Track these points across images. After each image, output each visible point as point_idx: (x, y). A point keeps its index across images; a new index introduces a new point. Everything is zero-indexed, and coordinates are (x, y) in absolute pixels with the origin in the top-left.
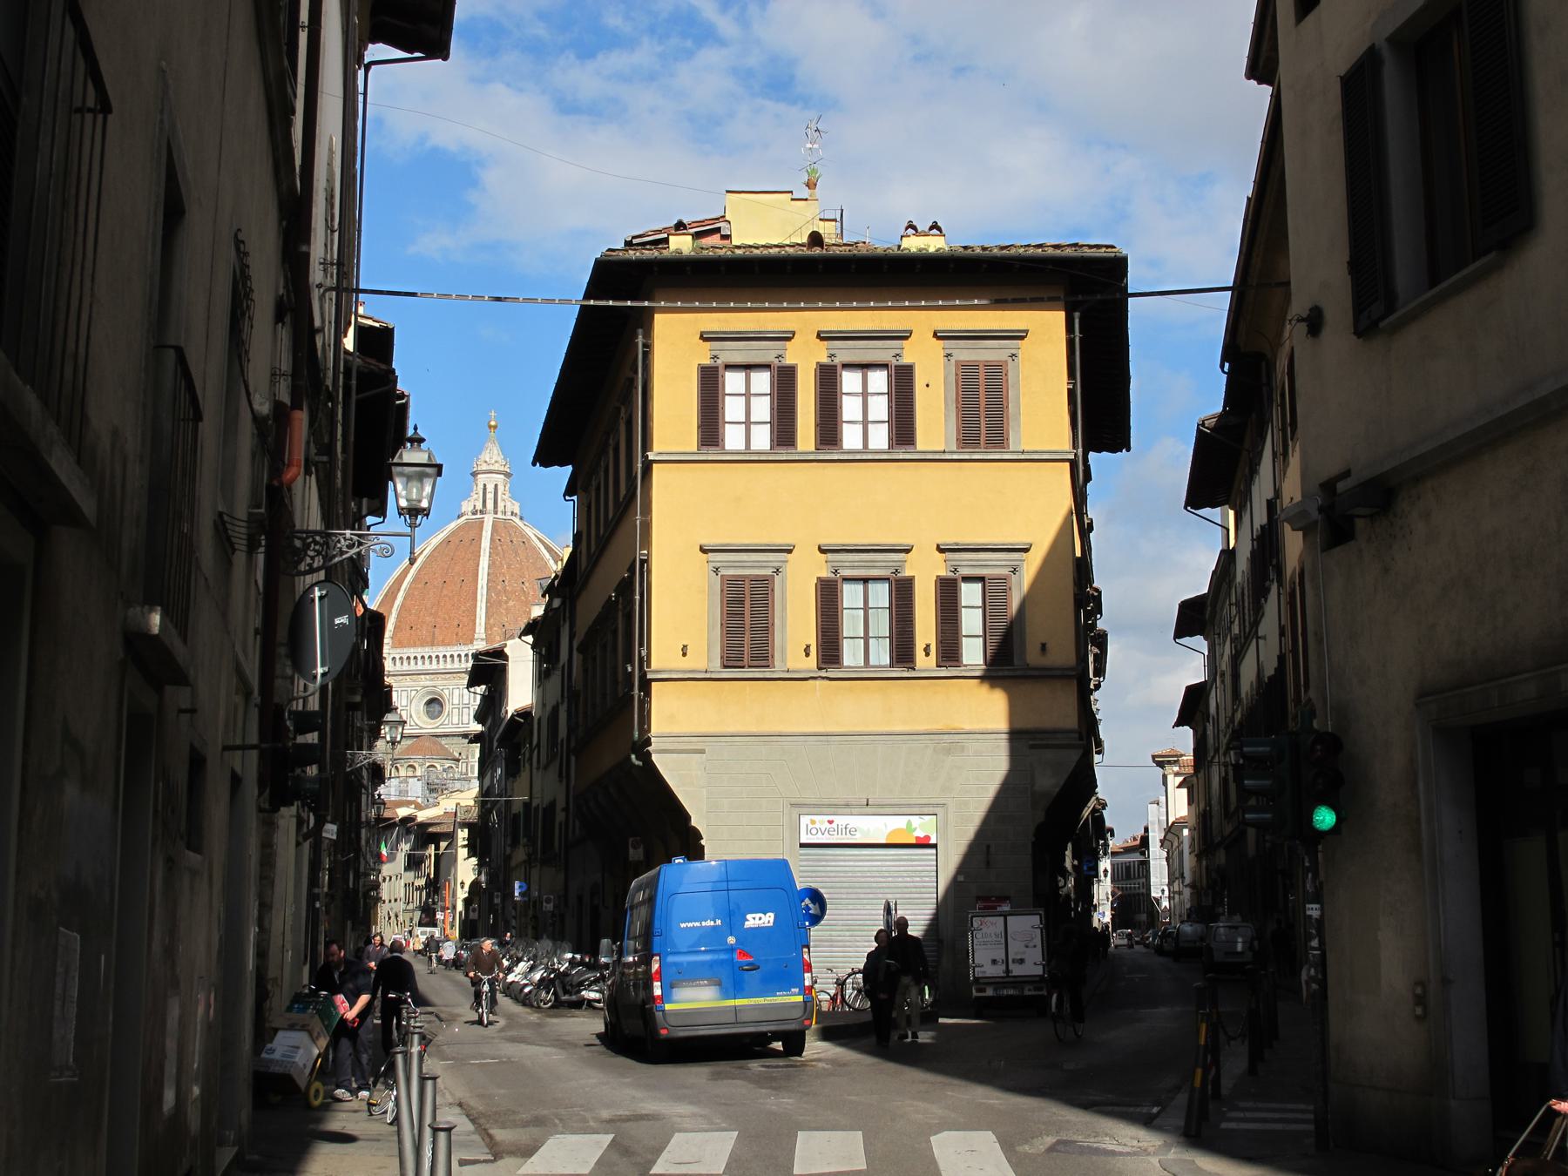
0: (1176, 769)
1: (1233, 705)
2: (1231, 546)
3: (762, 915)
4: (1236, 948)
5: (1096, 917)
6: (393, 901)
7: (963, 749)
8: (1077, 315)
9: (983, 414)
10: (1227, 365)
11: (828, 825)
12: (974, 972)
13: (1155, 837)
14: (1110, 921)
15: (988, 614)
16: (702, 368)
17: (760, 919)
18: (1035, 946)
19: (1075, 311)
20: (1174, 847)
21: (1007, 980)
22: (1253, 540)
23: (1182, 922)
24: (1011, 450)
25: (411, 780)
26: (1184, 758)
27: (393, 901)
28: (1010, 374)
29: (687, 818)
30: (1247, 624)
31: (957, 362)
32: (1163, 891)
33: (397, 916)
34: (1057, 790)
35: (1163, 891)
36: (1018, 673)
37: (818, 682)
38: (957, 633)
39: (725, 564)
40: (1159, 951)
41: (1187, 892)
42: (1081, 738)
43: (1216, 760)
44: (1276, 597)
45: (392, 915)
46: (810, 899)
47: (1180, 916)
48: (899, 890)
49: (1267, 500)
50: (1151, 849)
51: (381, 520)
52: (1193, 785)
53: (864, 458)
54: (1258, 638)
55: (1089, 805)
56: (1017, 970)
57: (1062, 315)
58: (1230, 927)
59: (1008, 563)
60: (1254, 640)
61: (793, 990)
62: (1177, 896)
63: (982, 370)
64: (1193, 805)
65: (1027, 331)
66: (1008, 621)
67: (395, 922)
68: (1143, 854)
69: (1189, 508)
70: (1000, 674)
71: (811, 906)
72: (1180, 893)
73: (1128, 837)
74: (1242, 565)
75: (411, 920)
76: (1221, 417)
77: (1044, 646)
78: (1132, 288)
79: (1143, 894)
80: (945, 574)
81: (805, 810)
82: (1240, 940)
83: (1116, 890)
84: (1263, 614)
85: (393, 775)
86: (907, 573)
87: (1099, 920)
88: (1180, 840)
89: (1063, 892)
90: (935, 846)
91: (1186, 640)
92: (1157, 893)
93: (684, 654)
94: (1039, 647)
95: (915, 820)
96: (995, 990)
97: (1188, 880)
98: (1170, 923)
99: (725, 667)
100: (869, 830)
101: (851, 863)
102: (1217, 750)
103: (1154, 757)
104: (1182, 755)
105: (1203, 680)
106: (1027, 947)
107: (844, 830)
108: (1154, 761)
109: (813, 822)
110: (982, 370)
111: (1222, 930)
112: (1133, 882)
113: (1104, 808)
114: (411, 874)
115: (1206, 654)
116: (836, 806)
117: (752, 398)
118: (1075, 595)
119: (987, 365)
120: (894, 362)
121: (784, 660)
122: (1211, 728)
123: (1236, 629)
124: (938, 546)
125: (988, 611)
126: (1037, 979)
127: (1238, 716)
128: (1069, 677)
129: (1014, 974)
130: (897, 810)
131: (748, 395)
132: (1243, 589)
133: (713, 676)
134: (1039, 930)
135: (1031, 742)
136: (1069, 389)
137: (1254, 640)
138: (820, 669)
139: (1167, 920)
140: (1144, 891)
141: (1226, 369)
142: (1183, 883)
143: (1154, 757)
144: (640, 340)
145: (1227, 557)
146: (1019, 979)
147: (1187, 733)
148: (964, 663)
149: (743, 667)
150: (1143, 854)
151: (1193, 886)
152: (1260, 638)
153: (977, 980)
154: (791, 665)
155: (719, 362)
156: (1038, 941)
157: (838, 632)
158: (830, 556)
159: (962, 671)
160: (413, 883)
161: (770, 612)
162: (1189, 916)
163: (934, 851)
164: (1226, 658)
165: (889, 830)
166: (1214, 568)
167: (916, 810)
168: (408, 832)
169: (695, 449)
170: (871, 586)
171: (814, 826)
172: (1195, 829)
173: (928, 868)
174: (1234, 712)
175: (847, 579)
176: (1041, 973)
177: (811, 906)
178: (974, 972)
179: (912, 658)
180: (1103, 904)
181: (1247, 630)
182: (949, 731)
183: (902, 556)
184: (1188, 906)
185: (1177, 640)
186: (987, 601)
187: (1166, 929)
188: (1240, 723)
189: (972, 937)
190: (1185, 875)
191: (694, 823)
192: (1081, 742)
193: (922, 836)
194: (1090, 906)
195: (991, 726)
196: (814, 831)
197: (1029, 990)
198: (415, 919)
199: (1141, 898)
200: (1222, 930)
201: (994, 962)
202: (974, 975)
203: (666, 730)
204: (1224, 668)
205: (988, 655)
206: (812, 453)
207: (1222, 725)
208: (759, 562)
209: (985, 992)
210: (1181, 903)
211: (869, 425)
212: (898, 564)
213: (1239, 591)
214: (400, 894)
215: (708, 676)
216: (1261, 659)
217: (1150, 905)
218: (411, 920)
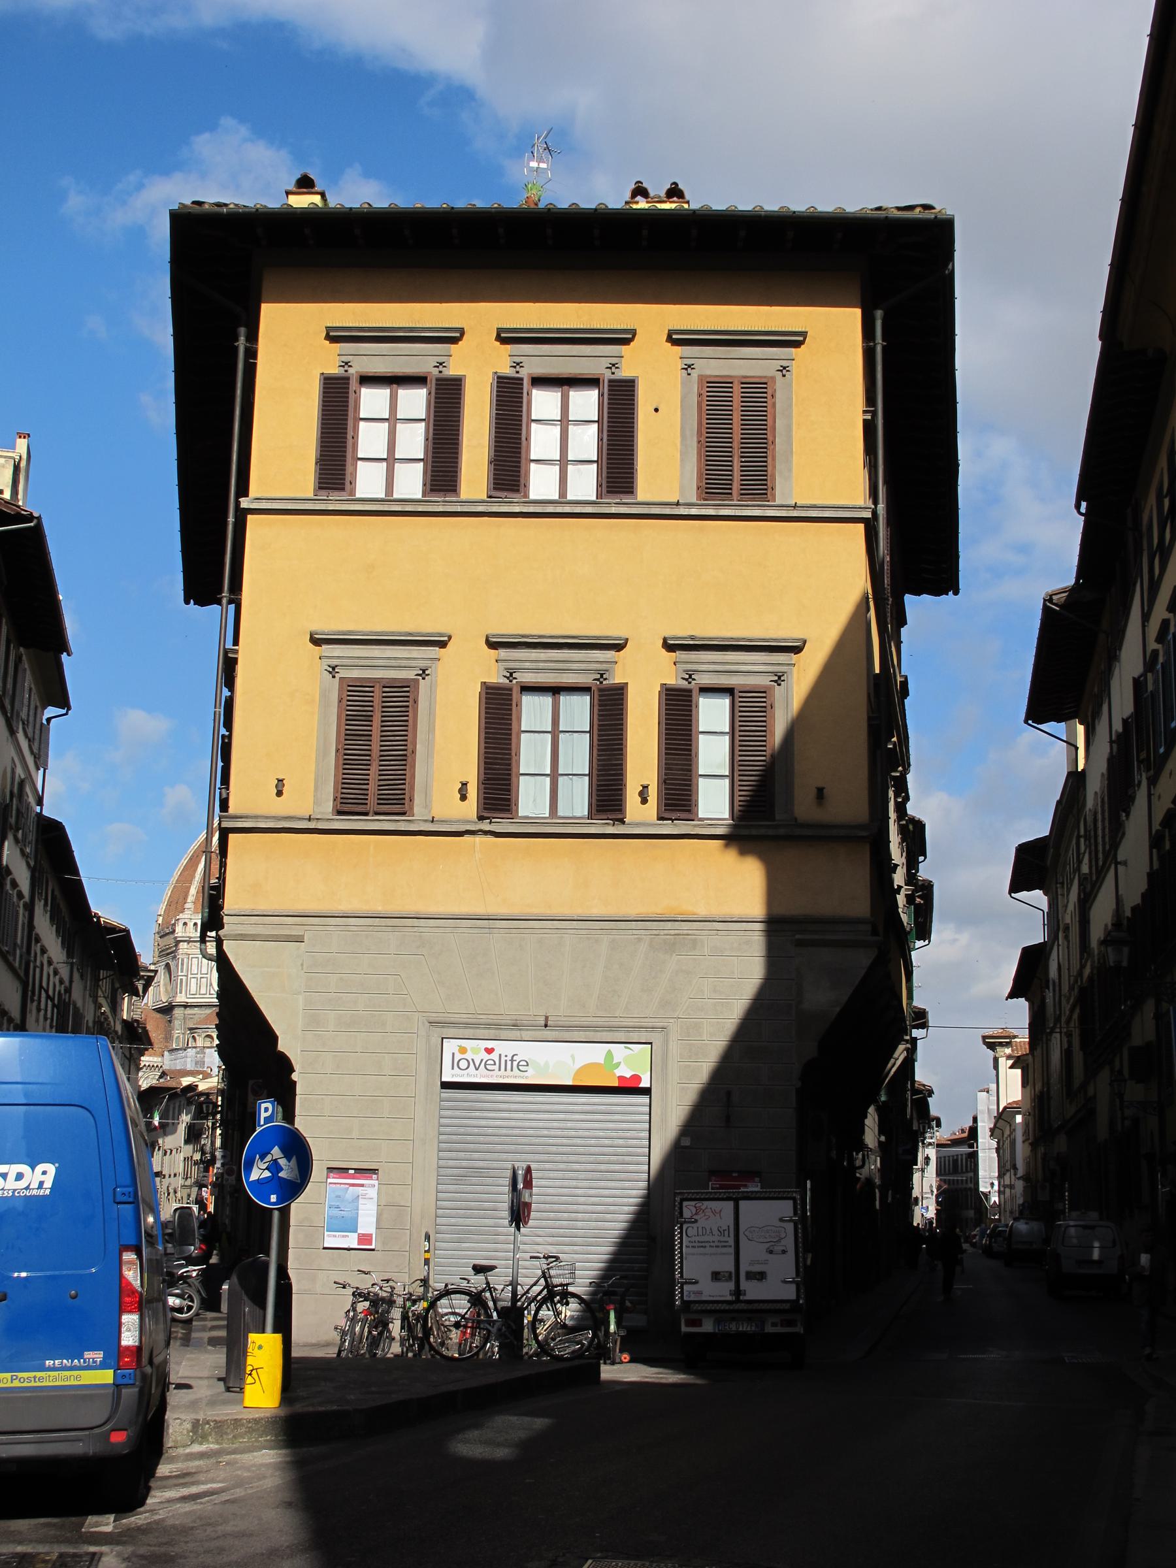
0: (1008, 1051)
1: (1081, 959)
2: (1081, 767)
3: (24, 1168)
4: (1091, 1254)
5: (918, 1211)
6: (172, 1176)
7: (695, 942)
8: (879, 314)
9: (736, 453)
10: (1084, 504)
11: (486, 1056)
12: (682, 1293)
13: (984, 1127)
14: (934, 1216)
15: (737, 743)
16: (325, 379)
17: (19, 1176)
18: (784, 1252)
19: (877, 308)
20: (1005, 1136)
21: (738, 1308)
22: (1111, 742)
23: (1015, 1219)
24: (778, 502)
25: (207, 1051)
26: (1016, 1040)
27: (172, 1176)
28: (778, 395)
29: (275, 1038)
30: (1101, 856)
32: (992, 1184)
33: (175, 1192)
34: (838, 1009)
35: (992, 1184)
36: (782, 831)
37: (478, 839)
38: (690, 770)
39: (346, 662)
40: (988, 1252)
41: (1020, 1185)
42: (875, 932)
44: (1146, 799)
45: (171, 1191)
46: (282, 1150)
47: (1011, 1212)
48: (592, 1158)
49: (1134, 679)
50: (980, 1140)
51: (64, 711)
52: (1028, 1065)
54: (1117, 863)
55: (896, 1055)
56: (753, 1291)
57: (857, 312)
58: (1085, 1227)
59: (770, 668)
60: (1113, 866)
61: (88, 1355)
62: (1008, 1191)
63: (737, 389)
64: (1028, 1088)
65: (804, 334)
66: (768, 758)
67: (174, 1198)
68: (971, 1146)
69: (1030, 722)
70: (754, 832)
71: (283, 1162)
72: (1011, 1187)
73: (956, 1129)
74: (1094, 786)
75: (189, 1196)
76: (1073, 591)
77: (820, 792)
78: (983, 1186)
79: (970, 1189)
80: (673, 682)
81: (451, 1032)
82: (1096, 1244)
83: (943, 1184)
84: (1124, 834)
85: (190, 1046)
86: (618, 680)
87: (923, 1215)
88: (1013, 1128)
89: (862, 1174)
90: (647, 1091)
91: (1022, 895)
92: (986, 1187)
93: (279, 793)
94: (813, 793)
95: (619, 1051)
96: (718, 1322)
97: (1020, 1173)
98: (999, 1220)
99: (340, 813)
101: (521, 1115)
102: (1058, 1019)
103: (984, 1038)
104: (1015, 1037)
105: (1043, 941)
106: (771, 1252)
107: (509, 1063)
108: (985, 1043)
109: (463, 1050)
110: (737, 389)
111: (1072, 1231)
112: (965, 1175)
113: (930, 1096)
114: (190, 1148)
115: (1046, 910)
116: (498, 1026)
117: (399, 426)
118: (869, 719)
119: (746, 383)
120: (608, 375)
121: (427, 806)
122: (1051, 994)
123: (1085, 869)
124: (665, 640)
125: (737, 738)
126: (787, 1306)
127: (1087, 971)
129: (748, 1297)
130: (591, 1035)
131: (392, 420)
132: (1095, 821)
133: (321, 826)
134: (791, 1225)
135: (798, 936)
136: (864, 420)
137: (1113, 866)
138: (481, 818)
139: (996, 1217)
140: (972, 1186)
141: (1083, 510)
142: (1015, 1175)
143: (984, 1038)
144: (242, 343)
145: (1076, 781)
146: (756, 1306)
147: (1022, 1004)
148: (700, 816)
149: (366, 814)
150: (971, 1146)
151: (1026, 1178)
152: (1120, 863)
153: (687, 1304)
154: (438, 811)
155: (351, 371)
156: (789, 1242)
157: (510, 765)
158: (503, 653)
159: (695, 826)
160: (192, 1157)
161: (410, 734)
162: (1021, 1212)
163: (644, 1099)
164: (1071, 907)
165: (579, 1064)
166: (1058, 798)
168: (189, 1102)
169: (310, 494)
170: (564, 699)
171: (463, 1056)
172: (1029, 1115)
173: (638, 1126)
174: (1083, 967)
175: (527, 689)
176: (793, 1296)
177: (283, 1162)
178: (682, 1293)
180: (927, 1198)
181: (1101, 863)
182: (672, 916)
183: (610, 655)
184: (1021, 1201)
185: (1013, 895)
186: (737, 724)
187: (996, 1227)
188: (1090, 978)
189: (681, 1233)
190: (1017, 1166)
191: (281, 1047)
193: (628, 1076)
194: (907, 1202)
195: (737, 911)
196: (463, 1064)
197: (774, 1325)
198: (192, 1196)
199: (969, 1193)
200: (1072, 1231)
201: (716, 1276)
202: (682, 1298)
203: (246, 906)
204: (1068, 920)
205: (736, 803)
207: (1065, 988)
208: (395, 658)
209: (700, 1325)
210: (1013, 1198)
211: (570, 467)
212: (604, 666)
213: (1090, 819)
214: (179, 1167)
215: (312, 825)
216: (1120, 893)
217: (979, 1200)
218: (189, 1196)
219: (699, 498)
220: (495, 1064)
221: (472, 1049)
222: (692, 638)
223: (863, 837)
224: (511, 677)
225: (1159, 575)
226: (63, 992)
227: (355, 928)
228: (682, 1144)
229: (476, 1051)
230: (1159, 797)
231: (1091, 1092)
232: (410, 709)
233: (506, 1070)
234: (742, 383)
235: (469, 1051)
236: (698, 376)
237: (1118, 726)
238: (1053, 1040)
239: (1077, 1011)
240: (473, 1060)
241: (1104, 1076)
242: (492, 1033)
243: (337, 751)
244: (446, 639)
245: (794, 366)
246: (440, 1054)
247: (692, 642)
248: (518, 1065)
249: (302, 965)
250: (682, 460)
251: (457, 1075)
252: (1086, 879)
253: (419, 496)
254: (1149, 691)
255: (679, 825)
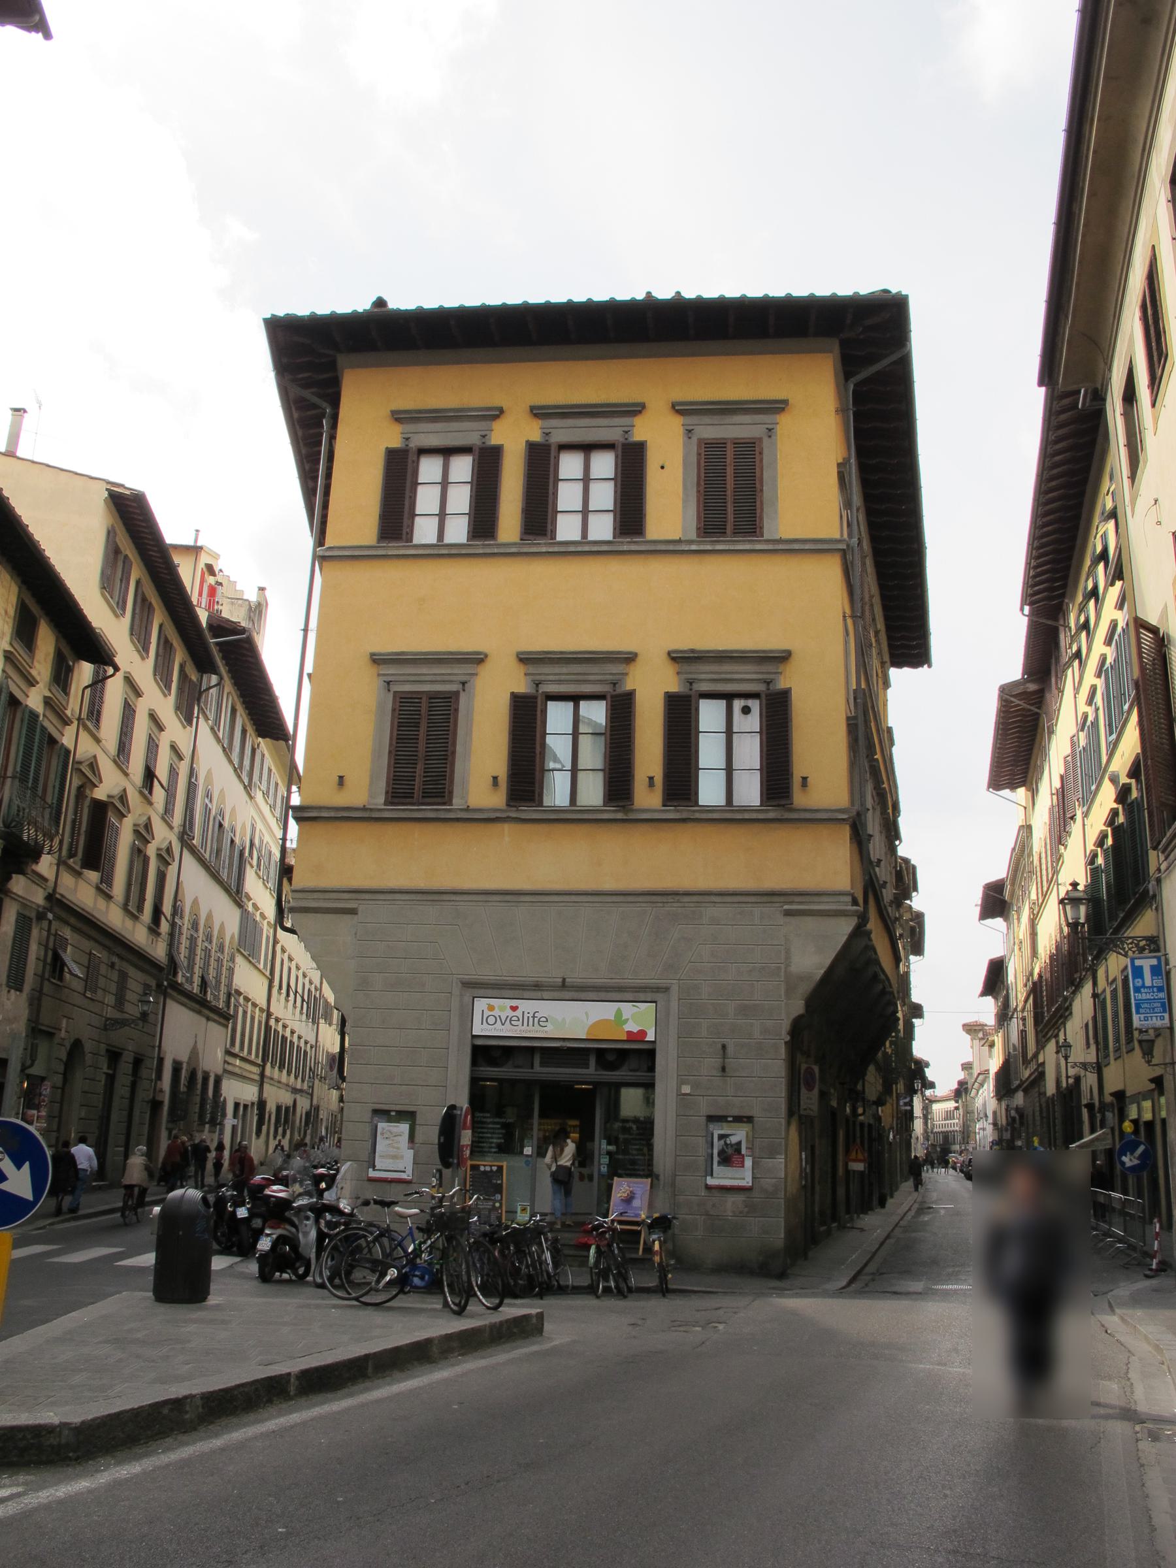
9: (730, 499)
11: (511, 1013)
31: (700, 441)
34: (822, 971)
42: (855, 902)
43: (1015, 1016)
53: (584, 550)
54: (1058, 885)
59: (761, 676)
69: (991, 790)
81: (481, 992)
86: (629, 686)
91: (989, 922)
95: (627, 1009)
100: (564, 1019)
107: (531, 1019)
109: (491, 1008)
119: (737, 443)
128: (950, 1100)
135: (786, 907)
147: (989, 1000)
167: (629, 996)
179: (629, 794)
181: (1050, 876)
185: (981, 922)
192: (855, 908)
204: (1021, 937)
206: (515, 544)
219: (698, 536)
220: (519, 1020)
221: (499, 1006)
222: (693, 651)
223: (843, 820)
224: (537, 684)
225: (1103, 593)
226: (313, 990)
227: (400, 903)
228: (683, 1092)
229: (502, 1009)
230: (1092, 826)
231: (1041, 1060)
232: (451, 716)
233: (528, 1025)
234: (735, 444)
235: (496, 1009)
236: (698, 439)
237: (1057, 784)
238: (1012, 1024)
239: (1031, 1000)
240: (499, 1016)
241: (1051, 1047)
242: (517, 993)
243: (390, 752)
244: (482, 656)
245: (779, 430)
246: (471, 1011)
247: (692, 655)
248: (539, 1021)
249: (356, 934)
250: (684, 507)
251: (487, 1030)
252: (1034, 903)
253: (465, 541)
254: (1081, 746)
255: (682, 810)
